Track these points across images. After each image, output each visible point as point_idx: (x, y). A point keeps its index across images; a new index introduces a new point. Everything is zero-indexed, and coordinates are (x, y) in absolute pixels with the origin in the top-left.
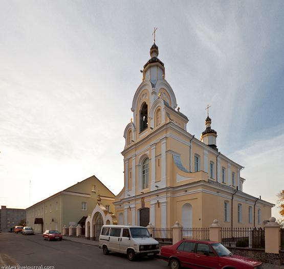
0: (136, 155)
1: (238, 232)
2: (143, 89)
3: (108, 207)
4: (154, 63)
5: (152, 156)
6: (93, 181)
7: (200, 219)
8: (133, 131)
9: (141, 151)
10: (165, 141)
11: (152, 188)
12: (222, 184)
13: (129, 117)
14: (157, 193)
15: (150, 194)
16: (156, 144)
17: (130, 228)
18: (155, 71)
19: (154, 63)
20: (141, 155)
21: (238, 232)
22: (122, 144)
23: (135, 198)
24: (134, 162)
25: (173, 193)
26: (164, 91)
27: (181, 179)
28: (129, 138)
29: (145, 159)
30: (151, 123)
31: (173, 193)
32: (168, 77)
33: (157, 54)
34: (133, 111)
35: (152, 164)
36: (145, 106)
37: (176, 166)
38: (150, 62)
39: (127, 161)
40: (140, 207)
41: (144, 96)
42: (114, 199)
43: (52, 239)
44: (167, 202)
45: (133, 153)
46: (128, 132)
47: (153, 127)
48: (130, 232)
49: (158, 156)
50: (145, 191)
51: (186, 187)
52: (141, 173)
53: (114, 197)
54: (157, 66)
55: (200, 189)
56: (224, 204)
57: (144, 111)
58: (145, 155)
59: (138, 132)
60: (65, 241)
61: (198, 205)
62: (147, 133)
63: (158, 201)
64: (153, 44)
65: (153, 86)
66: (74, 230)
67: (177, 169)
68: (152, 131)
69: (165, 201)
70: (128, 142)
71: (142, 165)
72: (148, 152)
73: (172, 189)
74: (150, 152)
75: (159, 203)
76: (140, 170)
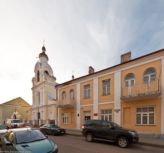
0: (36, 91)
3: (104, 94)
4: (43, 55)
6: (19, 100)
7: (78, 115)
9: (38, 89)
10: (44, 88)
13: (34, 75)
17: (147, 116)
18: (44, 58)
19: (43, 55)
22: (31, 85)
23: (36, 108)
24: (35, 93)
25: (48, 107)
26: (46, 67)
27: (50, 103)
30: (40, 80)
32: (49, 62)
33: (45, 51)
34: (35, 72)
36: (39, 72)
37: (48, 98)
38: (41, 54)
39: (33, 92)
42: (29, 108)
44: (45, 111)
45: (35, 90)
46: (33, 80)
52: (38, 98)
53: (30, 106)
54: (44, 56)
55: (54, 107)
57: (38, 74)
60: (68, 136)
62: (39, 83)
64: (43, 46)
65: (41, 65)
66: (106, 118)
67: (48, 99)
68: (40, 83)
70: (34, 85)
72: (39, 91)
73: (47, 106)
76: (38, 97)
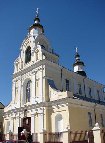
1: (82, 133)
2: (29, 38)
5: (33, 79)
8: (20, 63)
11: (33, 102)
12: (90, 98)
14: (37, 105)
15: (32, 107)
16: (36, 72)
20: (25, 79)
21: (82, 134)
23: (20, 110)
28: (18, 67)
29: (29, 82)
30: (33, 58)
31: (47, 104)
35: (33, 85)
40: (22, 116)
41: (29, 43)
43: (73, 77)
47: (34, 61)
48: (31, 26)
49: (36, 80)
50: (28, 104)
51: (58, 102)
56: (87, 115)
58: (29, 79)
59: (24, 63)
61: (66, 115)
63: (37, 112)
69: (42, 112)
71: (26, 85)
72: (30, 77)
74: (32, 77)
75: (37, 114)
